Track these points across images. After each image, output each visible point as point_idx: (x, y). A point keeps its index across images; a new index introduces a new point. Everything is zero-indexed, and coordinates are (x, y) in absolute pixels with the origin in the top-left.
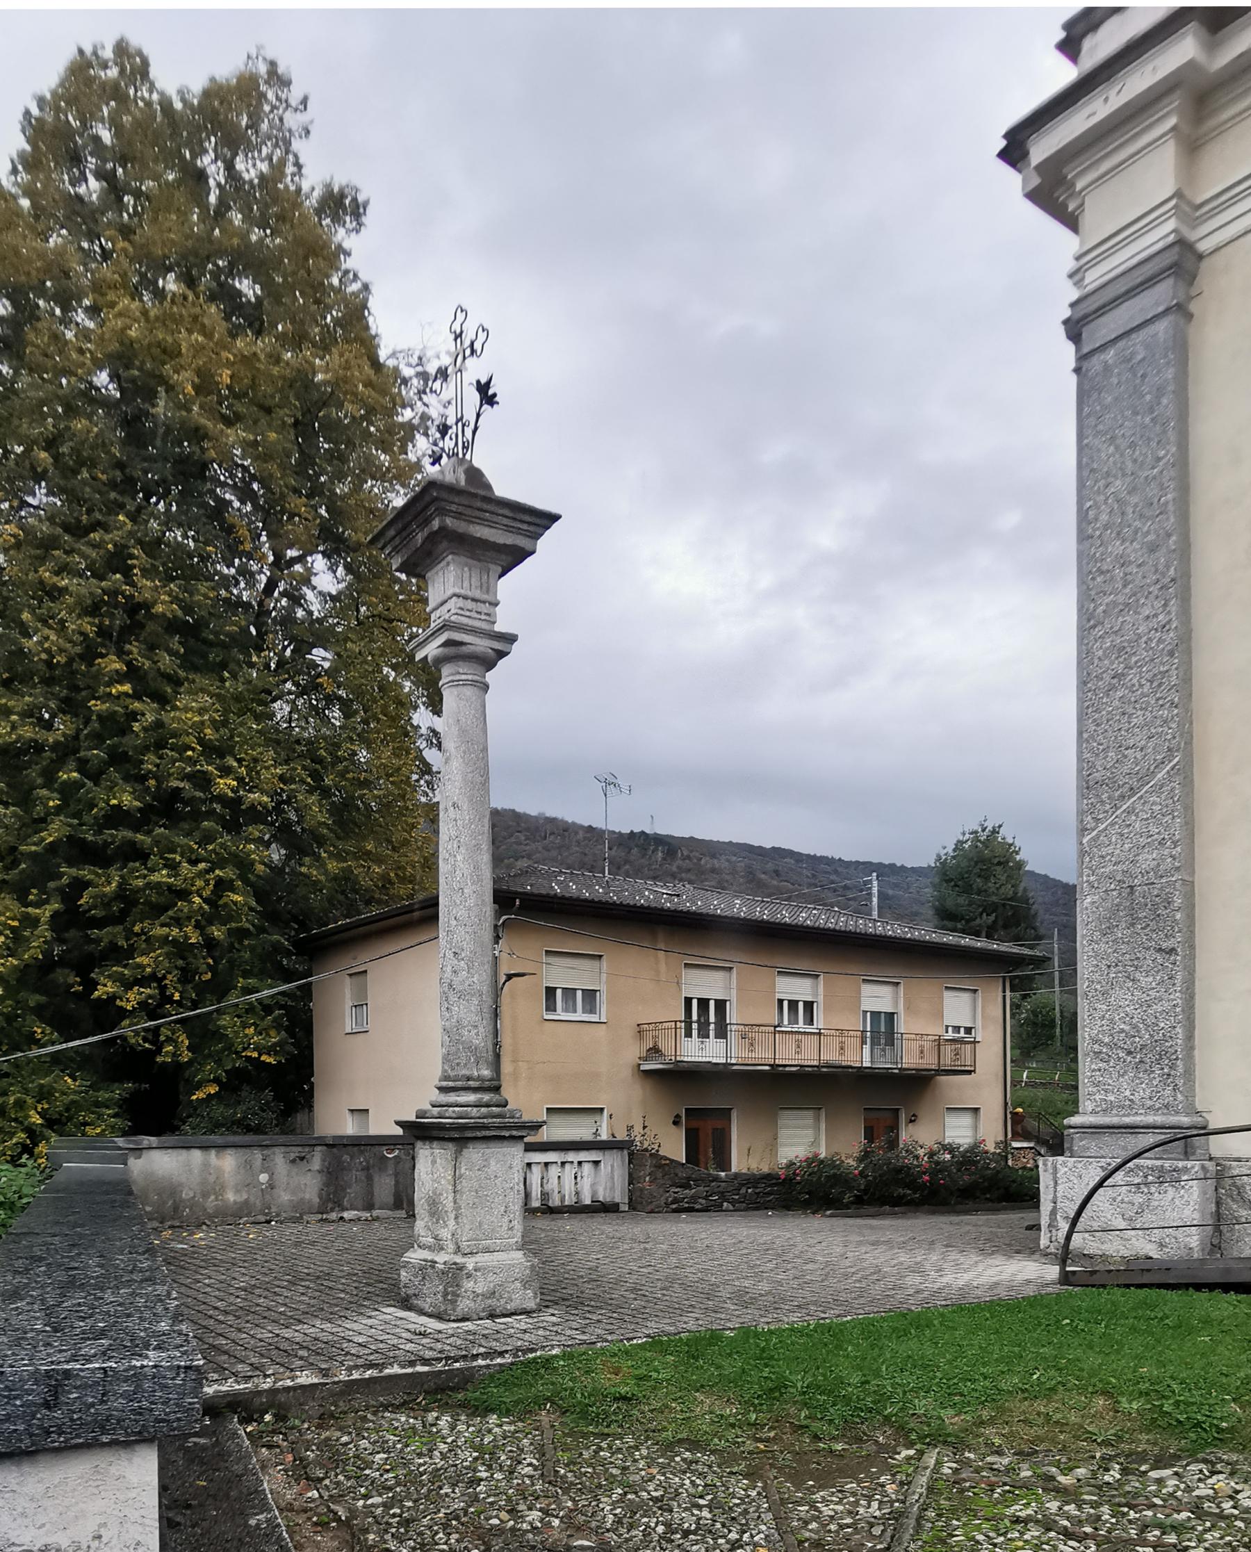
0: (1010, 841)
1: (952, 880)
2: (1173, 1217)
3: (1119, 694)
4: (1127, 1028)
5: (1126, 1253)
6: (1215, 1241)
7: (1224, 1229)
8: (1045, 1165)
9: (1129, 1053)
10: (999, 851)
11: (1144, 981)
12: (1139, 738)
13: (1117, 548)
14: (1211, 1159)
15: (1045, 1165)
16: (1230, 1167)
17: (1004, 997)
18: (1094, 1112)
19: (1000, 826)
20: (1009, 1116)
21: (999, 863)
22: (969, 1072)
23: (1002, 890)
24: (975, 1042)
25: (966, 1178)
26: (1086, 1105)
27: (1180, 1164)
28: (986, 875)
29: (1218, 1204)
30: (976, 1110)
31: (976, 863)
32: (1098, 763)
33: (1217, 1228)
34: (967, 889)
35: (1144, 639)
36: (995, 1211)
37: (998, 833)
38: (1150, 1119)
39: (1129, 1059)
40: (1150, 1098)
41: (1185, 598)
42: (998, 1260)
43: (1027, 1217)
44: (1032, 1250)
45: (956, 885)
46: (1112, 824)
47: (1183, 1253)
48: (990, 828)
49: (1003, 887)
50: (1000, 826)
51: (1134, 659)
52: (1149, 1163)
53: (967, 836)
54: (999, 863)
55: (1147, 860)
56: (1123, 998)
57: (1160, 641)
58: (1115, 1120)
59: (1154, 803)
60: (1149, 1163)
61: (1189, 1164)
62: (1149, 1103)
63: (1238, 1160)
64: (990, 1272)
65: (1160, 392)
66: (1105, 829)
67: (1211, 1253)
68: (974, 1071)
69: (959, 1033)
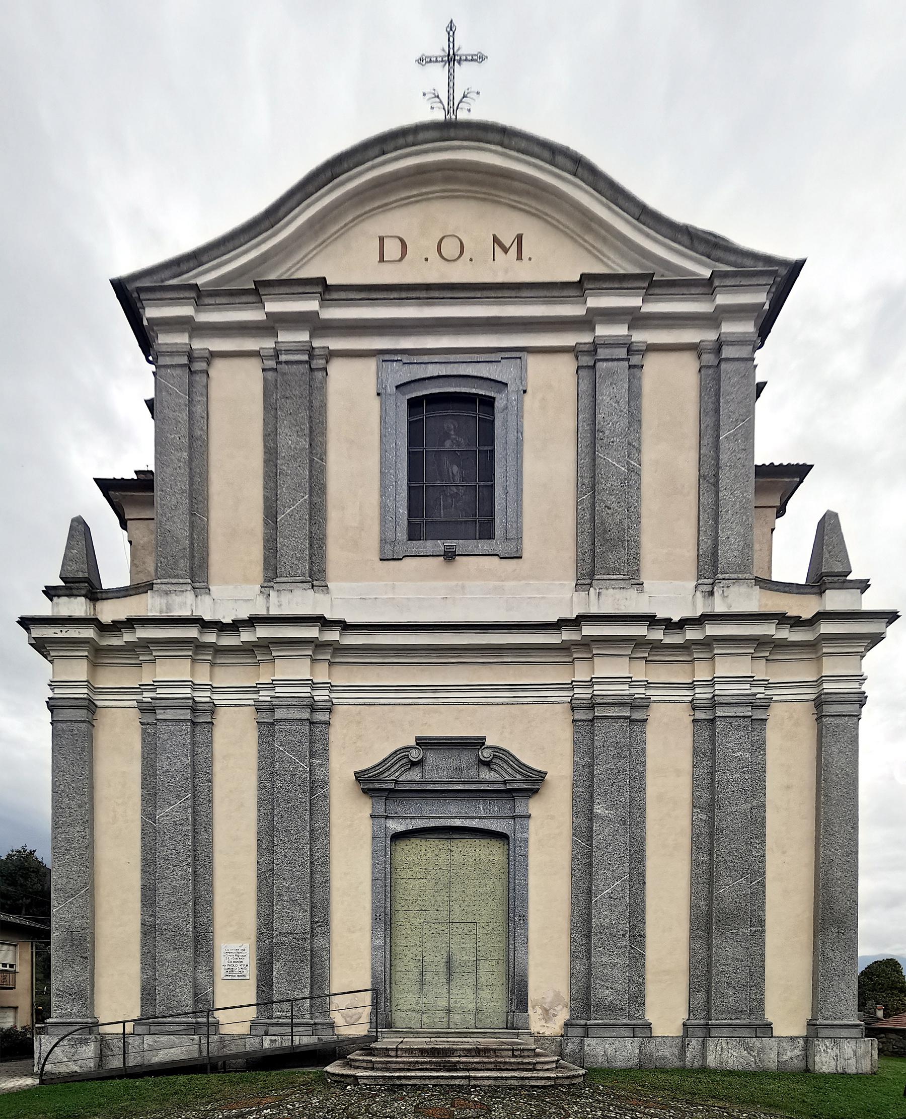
0: (40, 861)
1: (4, 876)
2: (85, 1056)
3: (67, 857)
4: (70, 985)
5: (68, 1071)
6: (100, 1064)
7: (103, 1059)
8: (36, 1039)
9: (70, 995)
10: (33, 865)
11: (76, 968)
12: (75, 876)
13: (66, 800)
14: (99, 1034)
15: (36, 1039)
16: (105, 1037)
17: (32, 952)
18: (56, 1017)
19: (34, 851)
20: (34, 1011)
21: (33, 872)
22: (11, 989)
23: (35, 887)
24: (15, 972)
25: (5, 1044)
26: (54, 1015)
27: (88, 1037)
28: (26, 877)
29: (101, 1050)
30: (16, 1008)
31: (20, 869)
32: (59, 881)
33: (101, 1060)
34: (13, 883)
35: (77, 839)
36: (20, 1059)
37: (33, 854)
38: (78, 1020)
39: (70, 997)
40: (78, 1012)
41: (92, 829)
42: (17, 1079)
43: (30, 1061)
44: (31, 1074)
45: (7, 879)
46: (64, 906)
47: (88, 1069)
48: (28, 851)
49: (36, 885)
50: (34, 851)
51: (73, 846)
52: (77, 1036)
53: (14, 853)
54: (33, 872)
55: (78, 922)
56: (68, 973)
57: (82, 842)
58: (64, 1021)
59: (80, 902)
60: (77, 1036)
61: (91, 1037)
62: (78, 1014)
63: (108, 1034)
64: (13, 1083)
65: (83, 749)
66: (62, 908)
67: (98, 1068)
68: (15, 988)
69: (6, 967)
